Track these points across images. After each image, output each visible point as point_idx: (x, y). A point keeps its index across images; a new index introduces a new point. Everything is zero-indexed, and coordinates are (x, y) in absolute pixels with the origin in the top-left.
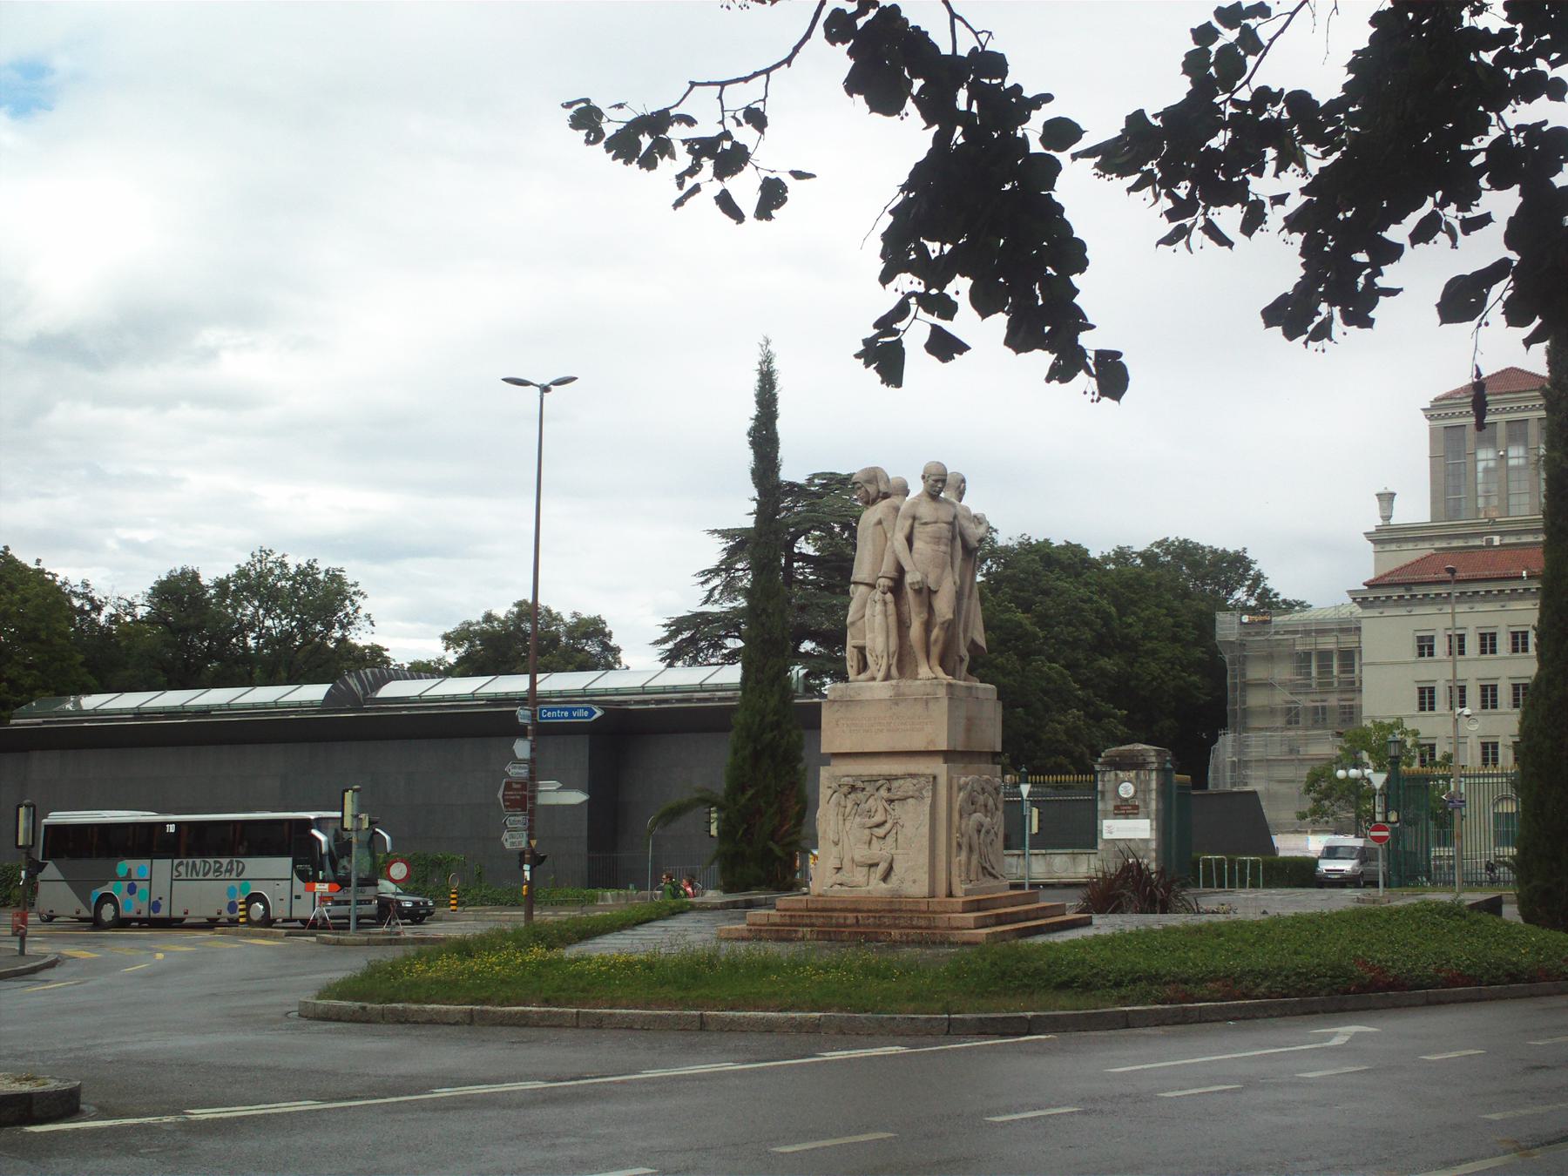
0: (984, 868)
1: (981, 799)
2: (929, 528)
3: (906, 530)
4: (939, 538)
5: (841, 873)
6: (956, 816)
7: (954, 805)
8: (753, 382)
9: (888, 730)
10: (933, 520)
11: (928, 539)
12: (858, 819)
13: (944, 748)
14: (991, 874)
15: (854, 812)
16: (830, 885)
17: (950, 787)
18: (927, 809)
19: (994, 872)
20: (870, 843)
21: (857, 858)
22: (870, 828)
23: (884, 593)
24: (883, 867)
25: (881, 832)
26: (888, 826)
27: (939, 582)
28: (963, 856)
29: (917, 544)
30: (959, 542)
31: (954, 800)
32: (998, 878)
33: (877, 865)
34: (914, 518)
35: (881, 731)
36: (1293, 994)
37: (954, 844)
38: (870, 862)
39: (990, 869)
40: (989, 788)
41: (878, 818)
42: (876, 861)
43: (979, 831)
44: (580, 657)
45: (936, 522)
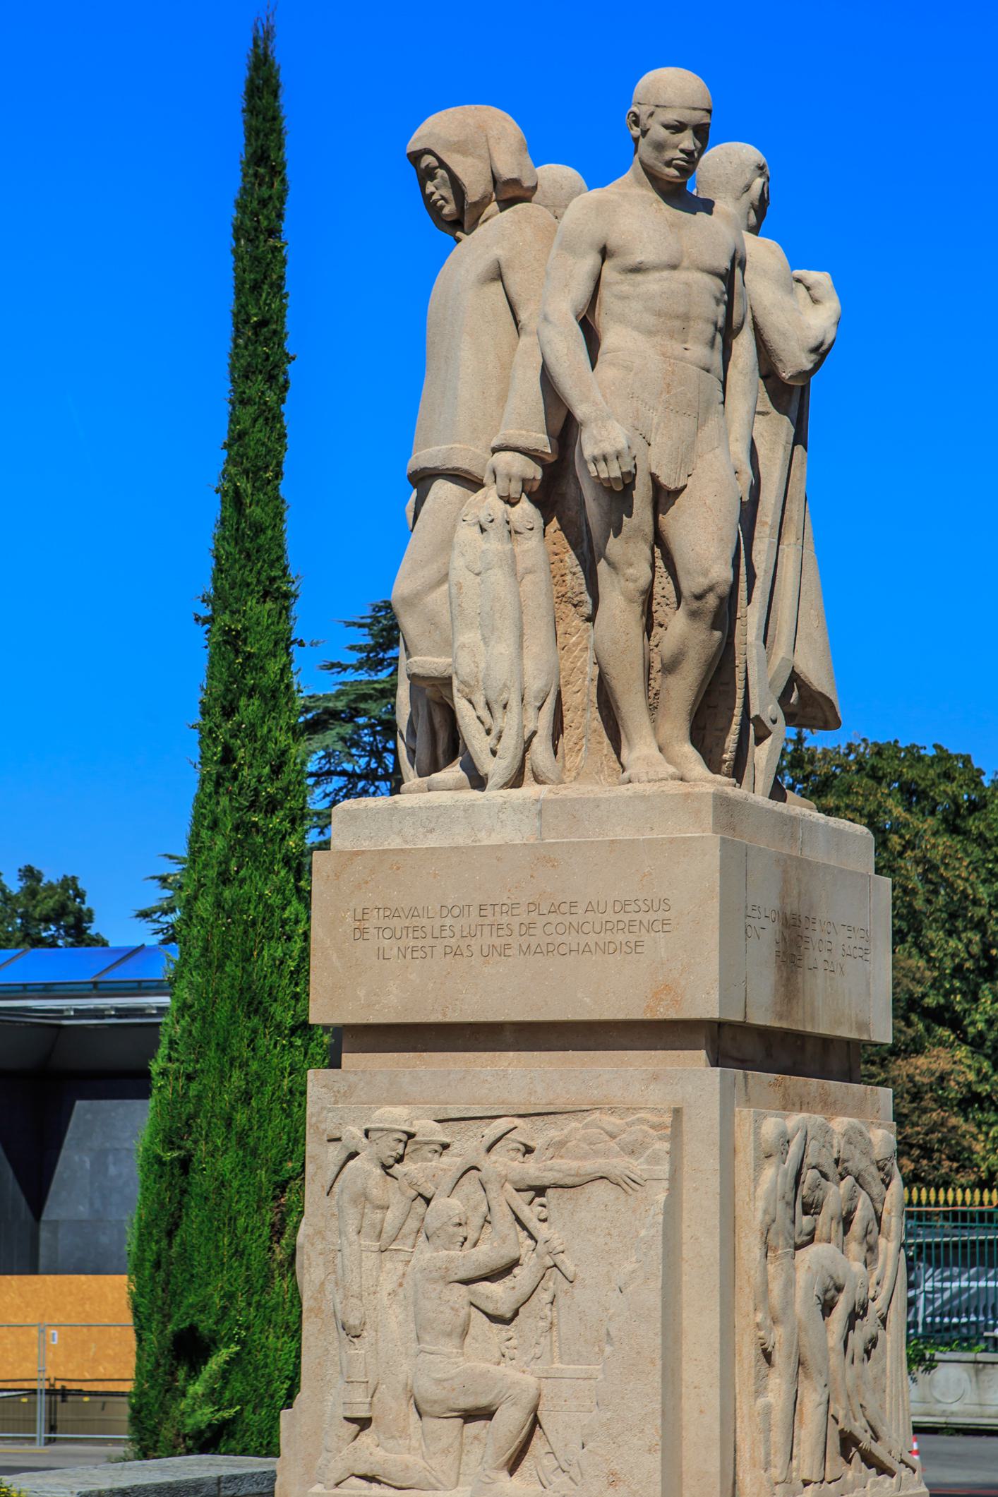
0: (848, 1442)
1: (835, 1195)
2: (652, 284)
3: (579, 291)
4: (686, 317)
5: (367, 1438)
6: (749, 1247)
7: (742, 1211)
8: (239, 75)
9: (526, 951)
10: (665, 258)
11: (650, 320)
12: (427, 1255)
13: (710, 1010)
14: (870, 1460)
15: (412, 1224)
16: (335, 1477)
17: (728, 1152)
18: (650, 1227)
19: (878, 1450)
20: (465, 1333)
21: (427, 1389)
22: (466, 1282)
23: (510, 501)
24: (509, 1421)
25: (499, 1294)
26: (523, 1277)
27: (686, 455)
28: (777, 1384)
29: (613, 337)
30: (744, 345)
31: (742, 1194)
32: (892, 1474)
33: (485, 1414)
34: (605, 253)
35: (504, 951)
36: (271, 952)
37: (748, 1352)
38: (467, 1402)
39: (866, 1441)
40: (877, 1059)
41: (486, 1254)
42: (483, 1401)
43: (827, 1308)
44: (299, 1032)
45: (674, 267)
